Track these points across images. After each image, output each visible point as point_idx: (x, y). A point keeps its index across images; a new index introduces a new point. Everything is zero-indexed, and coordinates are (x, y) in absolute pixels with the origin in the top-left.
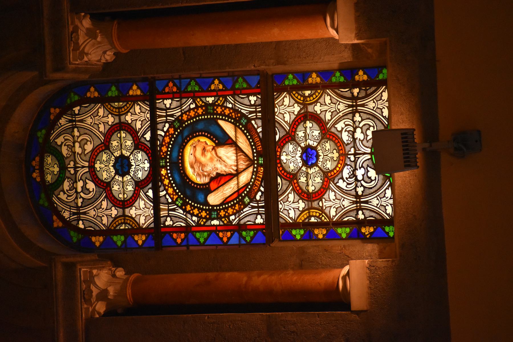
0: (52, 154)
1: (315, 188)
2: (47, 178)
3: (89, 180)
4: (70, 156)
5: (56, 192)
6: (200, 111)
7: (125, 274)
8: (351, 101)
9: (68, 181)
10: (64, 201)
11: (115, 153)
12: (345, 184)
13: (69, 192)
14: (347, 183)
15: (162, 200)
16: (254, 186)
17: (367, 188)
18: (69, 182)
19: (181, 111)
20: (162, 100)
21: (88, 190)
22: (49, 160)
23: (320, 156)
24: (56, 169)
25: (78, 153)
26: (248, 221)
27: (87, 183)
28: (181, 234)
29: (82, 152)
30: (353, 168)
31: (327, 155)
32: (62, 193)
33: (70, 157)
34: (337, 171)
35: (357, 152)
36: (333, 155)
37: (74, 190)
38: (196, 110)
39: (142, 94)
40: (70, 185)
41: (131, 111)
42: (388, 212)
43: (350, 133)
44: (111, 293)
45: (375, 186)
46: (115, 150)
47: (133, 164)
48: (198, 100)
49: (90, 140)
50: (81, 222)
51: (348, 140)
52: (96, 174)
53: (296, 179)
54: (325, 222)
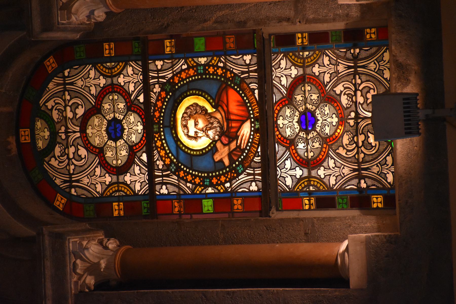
0: (41, 118)
1: (314, 154)
2: (38, 144)
3: (81, 146)
4: (351, 106)
8: (352, 62)
9: (59, 147)
10: (56, 167)
12: (57, 162)
16: (250, 152)
17: (77, 166)
18: (60, 147)
19: (173, 72)
20: (241, 56)
21: (80, 156)
22: (39, 124)
23: (318, 120)
24: (47, 134)
25: (359, 102)
27: (78, 149)
29: (73, 117)
30: (64, 146)
32: (53, 159)
37: (66, 156)
38: (187, 71)
40: (61, 150)
41: (318, 62)
42: (98, 190)
43: (349, 96)
44: (103, 265)
45: (85, 164)
47: (319, 118)
49: (81, 104)
51: (348, 104)
52: (88, 140)
53: (294, 145)
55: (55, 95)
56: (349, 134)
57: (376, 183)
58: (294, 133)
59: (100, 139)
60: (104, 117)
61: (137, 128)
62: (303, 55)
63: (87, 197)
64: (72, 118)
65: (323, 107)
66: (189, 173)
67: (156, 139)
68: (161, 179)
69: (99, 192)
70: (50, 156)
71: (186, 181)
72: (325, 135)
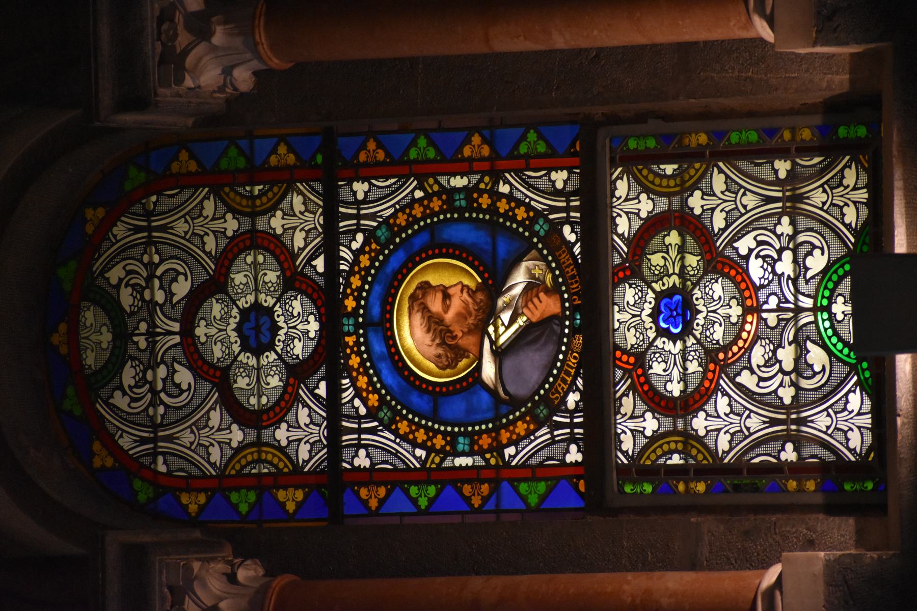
2: (85, 359)
3: (180, 363)
4: (770, 282)
5: (104, 393)
6: (436, 204)
7: (264, 576)
9: (132, 366)
10: (123, 411)
11: (239, 300)
12: (127, 399)
13: (135, 390)
14: (759, 377)
15: (346, 410)
18: (135, 368)
20: (545, 172)
21: (178, 386)
22: (89, 316)
23: (700, 312)
24: (106, 337)
26: (549, 459)
27: (175, 371)
28: (482, 486)
29: (166, 300)
31: (634, 316)
32: (118, 394)
33: (138, 311)
34: (740, 349)
35: (781, 305)
36: (207, 331)
37: (148, 386)
38: (426, 202)
39: (298, 164)
40: (137, 374)
43: (766, 262)
45: (188, 404)
46: (241, 293)
47: (281, 324)
48: (431, 181)
50: (160, 459)
51: (763, 277)
52: (197, 350)
54: (705, 465)
55: (756, 224)
56: (766, 344)
57: (391, 458)
58: (644, 339)
59: (638, 333)
60: (234, 303)
61: (730, 311)
62: (251, 191)
63: (190, 476)
64: (164, 304)
65: (710, 283)
66: (419, 425)
67: (348, 351)
68: (356, 436)
69: (855, 449)
70: (112, 385)
71: (415, 444)
72: (293, 359)
